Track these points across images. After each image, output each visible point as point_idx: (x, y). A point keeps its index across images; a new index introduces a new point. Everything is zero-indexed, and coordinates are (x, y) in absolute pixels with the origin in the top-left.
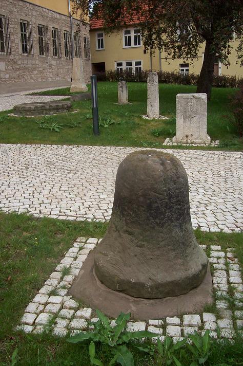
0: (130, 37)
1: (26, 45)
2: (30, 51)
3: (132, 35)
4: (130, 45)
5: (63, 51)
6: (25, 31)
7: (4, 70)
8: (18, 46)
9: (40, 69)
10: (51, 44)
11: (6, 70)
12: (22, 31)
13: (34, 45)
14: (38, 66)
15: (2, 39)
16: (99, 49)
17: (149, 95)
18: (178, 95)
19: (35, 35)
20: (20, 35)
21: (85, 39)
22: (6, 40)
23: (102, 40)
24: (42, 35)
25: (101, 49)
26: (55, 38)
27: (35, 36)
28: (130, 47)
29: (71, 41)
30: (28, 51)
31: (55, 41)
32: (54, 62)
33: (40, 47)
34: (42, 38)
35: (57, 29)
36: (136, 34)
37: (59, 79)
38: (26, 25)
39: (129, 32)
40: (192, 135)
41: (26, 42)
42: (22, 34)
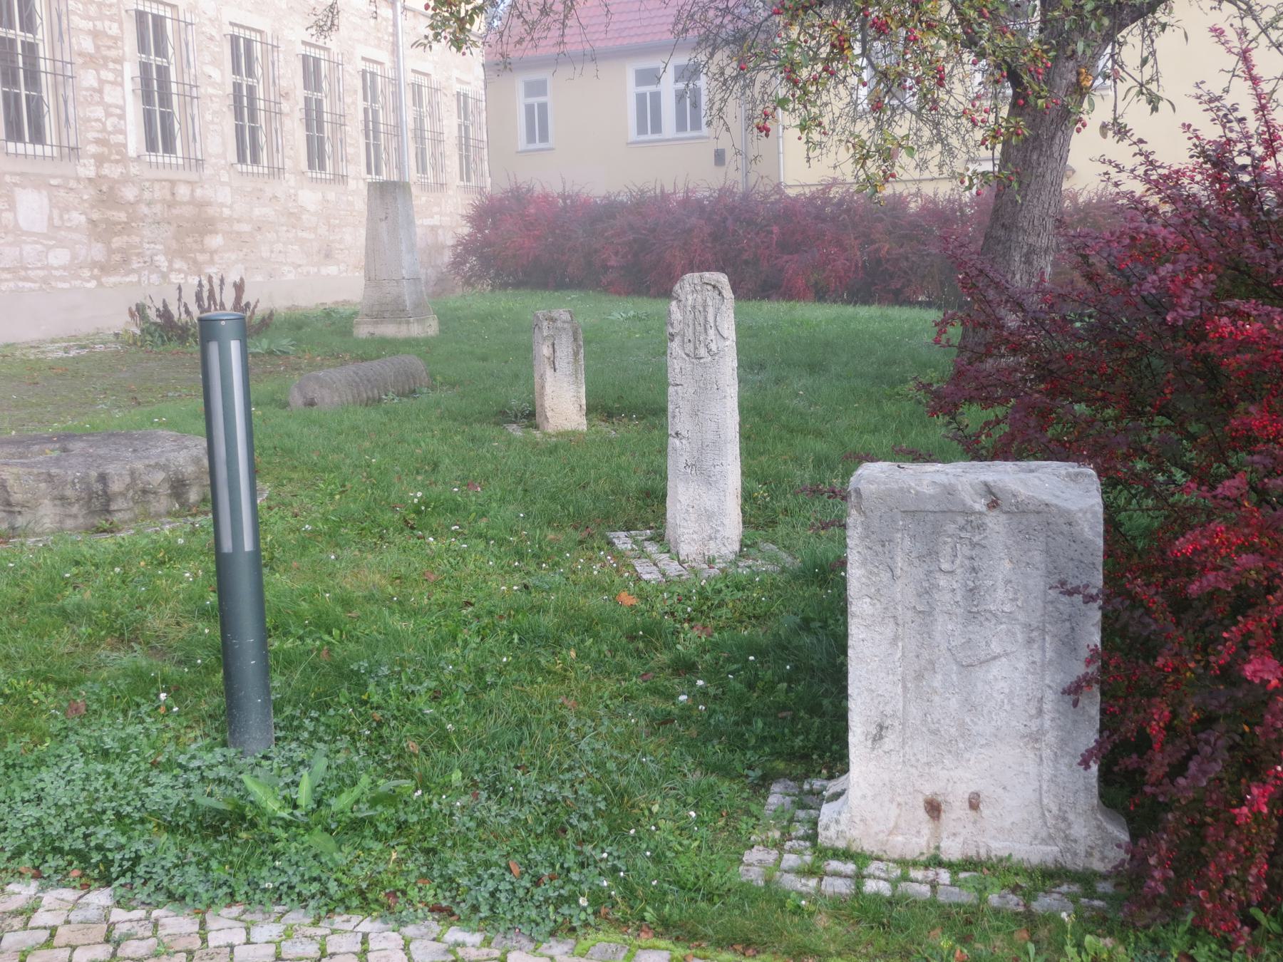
0: (656, 97)
1: (253, 132)
2: (186, 146)
3: (668, 87)
4: (657, 127)
5: (294, 133)
6: (250, 73)
7: (41, 227)
8: (122, 117)
9: (237, 227)
10: (299, 114)
11: (51, 224)
12: (142, 48)
13: (208, 117)
14: (226, 212)
15: (11, 80)
16: (531, 146)
17: (679, 399)
18: (873, 476)
19: (209, 70)
20: (131, 70)
21: (462, 99)
22: (183, 107)
23: (543, 107)
24: (318, 88)
25: (538, 145)
26: (374, 100)
27: (216, 76)
28: (656, 137)
29: (397, 109)
30: (264, 156)
31: (375, 112)
32: (310, 198)
33: (309, 139)
34: (319, 102)
35: (260, 32)
36: (681, 85)
37: (332, 270)
38: (257, 48)
39: (651, 77)
40: (974, 803)
41: (253, 118)
42: (145, 68)
